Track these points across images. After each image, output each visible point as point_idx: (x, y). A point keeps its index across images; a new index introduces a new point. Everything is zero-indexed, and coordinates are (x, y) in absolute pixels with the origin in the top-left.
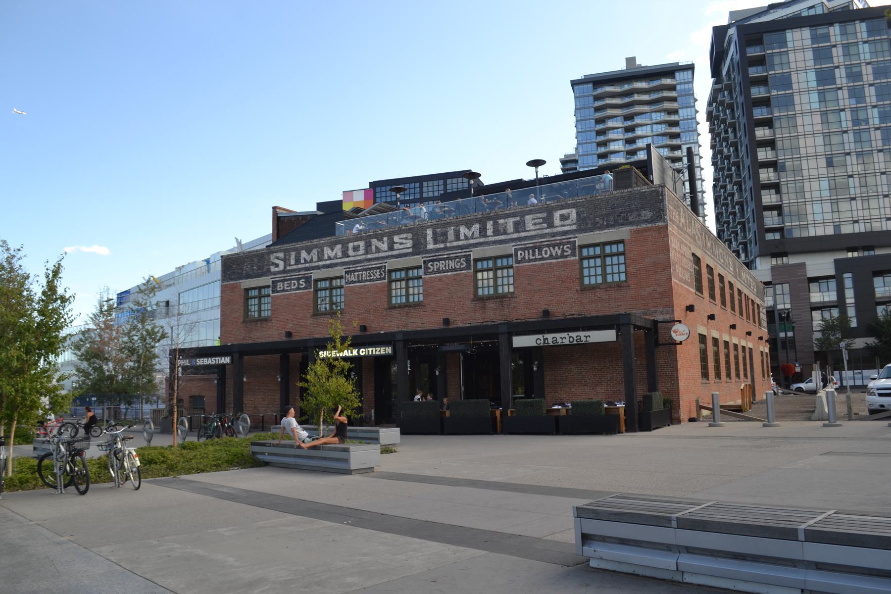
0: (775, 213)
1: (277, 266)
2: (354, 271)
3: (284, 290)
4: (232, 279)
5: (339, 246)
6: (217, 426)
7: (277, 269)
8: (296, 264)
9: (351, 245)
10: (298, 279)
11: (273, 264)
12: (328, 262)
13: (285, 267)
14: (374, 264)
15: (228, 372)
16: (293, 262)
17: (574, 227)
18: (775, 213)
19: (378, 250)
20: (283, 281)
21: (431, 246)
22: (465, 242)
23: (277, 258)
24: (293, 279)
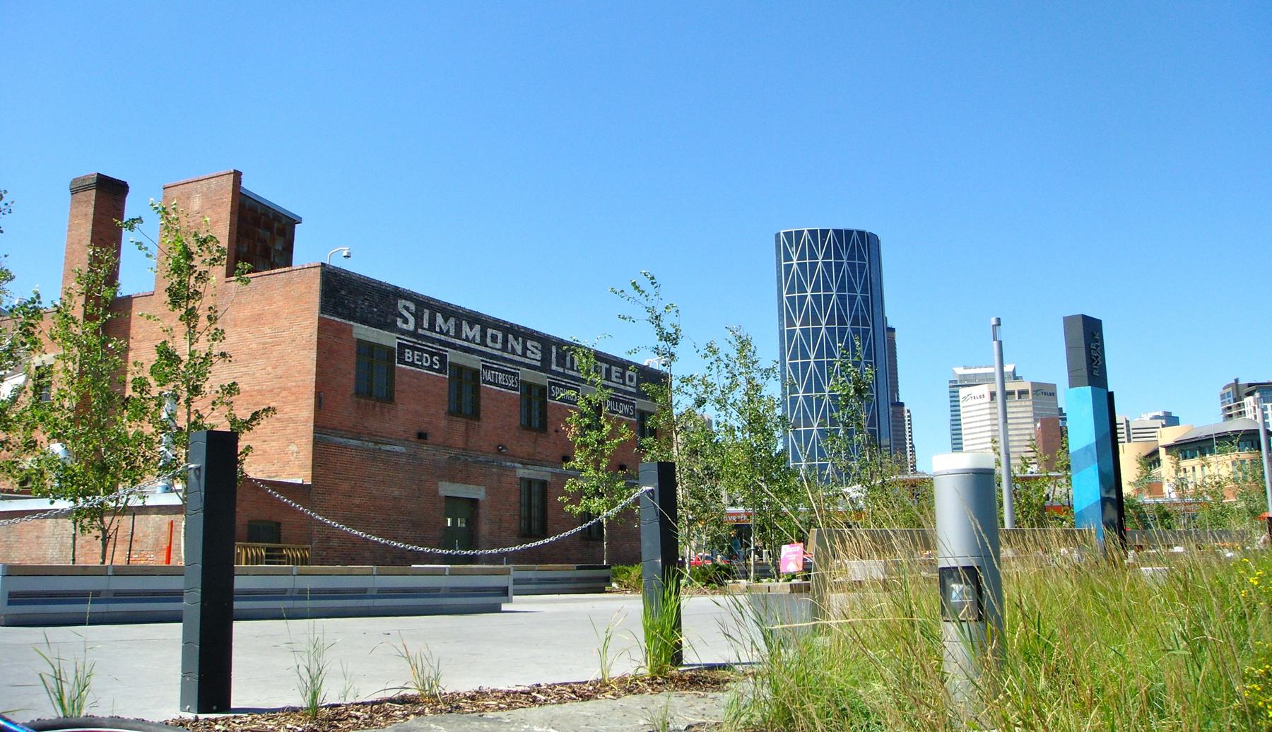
0: (963, 392)
1: (406, 321)
2: (492, 369)
3: (412, 364)
4: (339, 315)
5: (477, 327)
6: (838, 411)
7: (405, 326)
8: (429, 330)
9: (500, 336)
10: (432, 354)
11: (402, 316)
12: (466, 344)
13: (416, 328)
14: (508, 367)
15: (484, 512)
16: (426, 325)
17: (539, 364)
18: (963, 392)
19: (514, 352)
20: (413, 349)
21: (554, 367)
22: (438, 336)
23: (407, 309)
24: (426, 352)
